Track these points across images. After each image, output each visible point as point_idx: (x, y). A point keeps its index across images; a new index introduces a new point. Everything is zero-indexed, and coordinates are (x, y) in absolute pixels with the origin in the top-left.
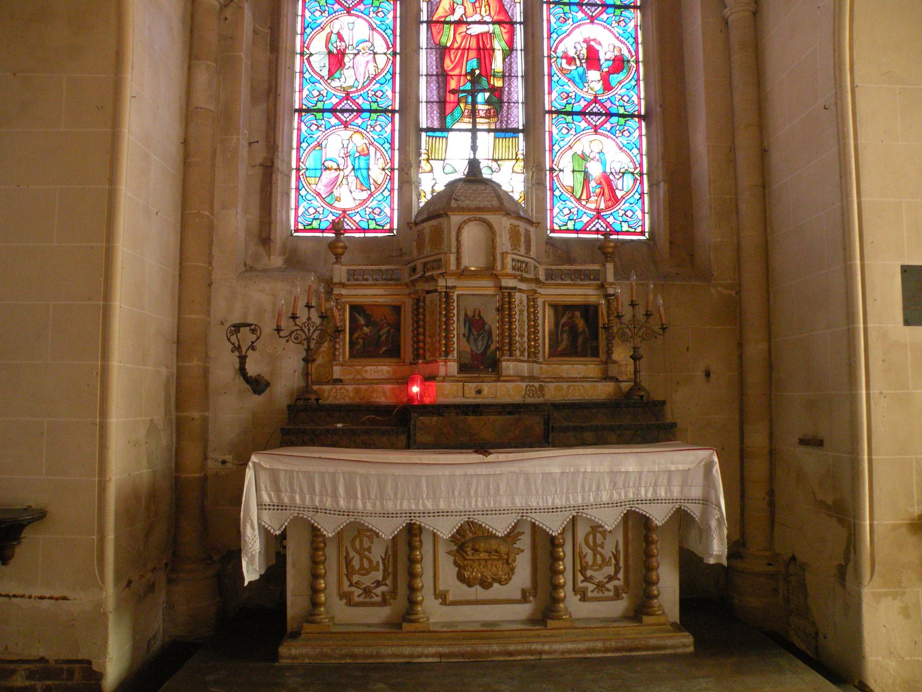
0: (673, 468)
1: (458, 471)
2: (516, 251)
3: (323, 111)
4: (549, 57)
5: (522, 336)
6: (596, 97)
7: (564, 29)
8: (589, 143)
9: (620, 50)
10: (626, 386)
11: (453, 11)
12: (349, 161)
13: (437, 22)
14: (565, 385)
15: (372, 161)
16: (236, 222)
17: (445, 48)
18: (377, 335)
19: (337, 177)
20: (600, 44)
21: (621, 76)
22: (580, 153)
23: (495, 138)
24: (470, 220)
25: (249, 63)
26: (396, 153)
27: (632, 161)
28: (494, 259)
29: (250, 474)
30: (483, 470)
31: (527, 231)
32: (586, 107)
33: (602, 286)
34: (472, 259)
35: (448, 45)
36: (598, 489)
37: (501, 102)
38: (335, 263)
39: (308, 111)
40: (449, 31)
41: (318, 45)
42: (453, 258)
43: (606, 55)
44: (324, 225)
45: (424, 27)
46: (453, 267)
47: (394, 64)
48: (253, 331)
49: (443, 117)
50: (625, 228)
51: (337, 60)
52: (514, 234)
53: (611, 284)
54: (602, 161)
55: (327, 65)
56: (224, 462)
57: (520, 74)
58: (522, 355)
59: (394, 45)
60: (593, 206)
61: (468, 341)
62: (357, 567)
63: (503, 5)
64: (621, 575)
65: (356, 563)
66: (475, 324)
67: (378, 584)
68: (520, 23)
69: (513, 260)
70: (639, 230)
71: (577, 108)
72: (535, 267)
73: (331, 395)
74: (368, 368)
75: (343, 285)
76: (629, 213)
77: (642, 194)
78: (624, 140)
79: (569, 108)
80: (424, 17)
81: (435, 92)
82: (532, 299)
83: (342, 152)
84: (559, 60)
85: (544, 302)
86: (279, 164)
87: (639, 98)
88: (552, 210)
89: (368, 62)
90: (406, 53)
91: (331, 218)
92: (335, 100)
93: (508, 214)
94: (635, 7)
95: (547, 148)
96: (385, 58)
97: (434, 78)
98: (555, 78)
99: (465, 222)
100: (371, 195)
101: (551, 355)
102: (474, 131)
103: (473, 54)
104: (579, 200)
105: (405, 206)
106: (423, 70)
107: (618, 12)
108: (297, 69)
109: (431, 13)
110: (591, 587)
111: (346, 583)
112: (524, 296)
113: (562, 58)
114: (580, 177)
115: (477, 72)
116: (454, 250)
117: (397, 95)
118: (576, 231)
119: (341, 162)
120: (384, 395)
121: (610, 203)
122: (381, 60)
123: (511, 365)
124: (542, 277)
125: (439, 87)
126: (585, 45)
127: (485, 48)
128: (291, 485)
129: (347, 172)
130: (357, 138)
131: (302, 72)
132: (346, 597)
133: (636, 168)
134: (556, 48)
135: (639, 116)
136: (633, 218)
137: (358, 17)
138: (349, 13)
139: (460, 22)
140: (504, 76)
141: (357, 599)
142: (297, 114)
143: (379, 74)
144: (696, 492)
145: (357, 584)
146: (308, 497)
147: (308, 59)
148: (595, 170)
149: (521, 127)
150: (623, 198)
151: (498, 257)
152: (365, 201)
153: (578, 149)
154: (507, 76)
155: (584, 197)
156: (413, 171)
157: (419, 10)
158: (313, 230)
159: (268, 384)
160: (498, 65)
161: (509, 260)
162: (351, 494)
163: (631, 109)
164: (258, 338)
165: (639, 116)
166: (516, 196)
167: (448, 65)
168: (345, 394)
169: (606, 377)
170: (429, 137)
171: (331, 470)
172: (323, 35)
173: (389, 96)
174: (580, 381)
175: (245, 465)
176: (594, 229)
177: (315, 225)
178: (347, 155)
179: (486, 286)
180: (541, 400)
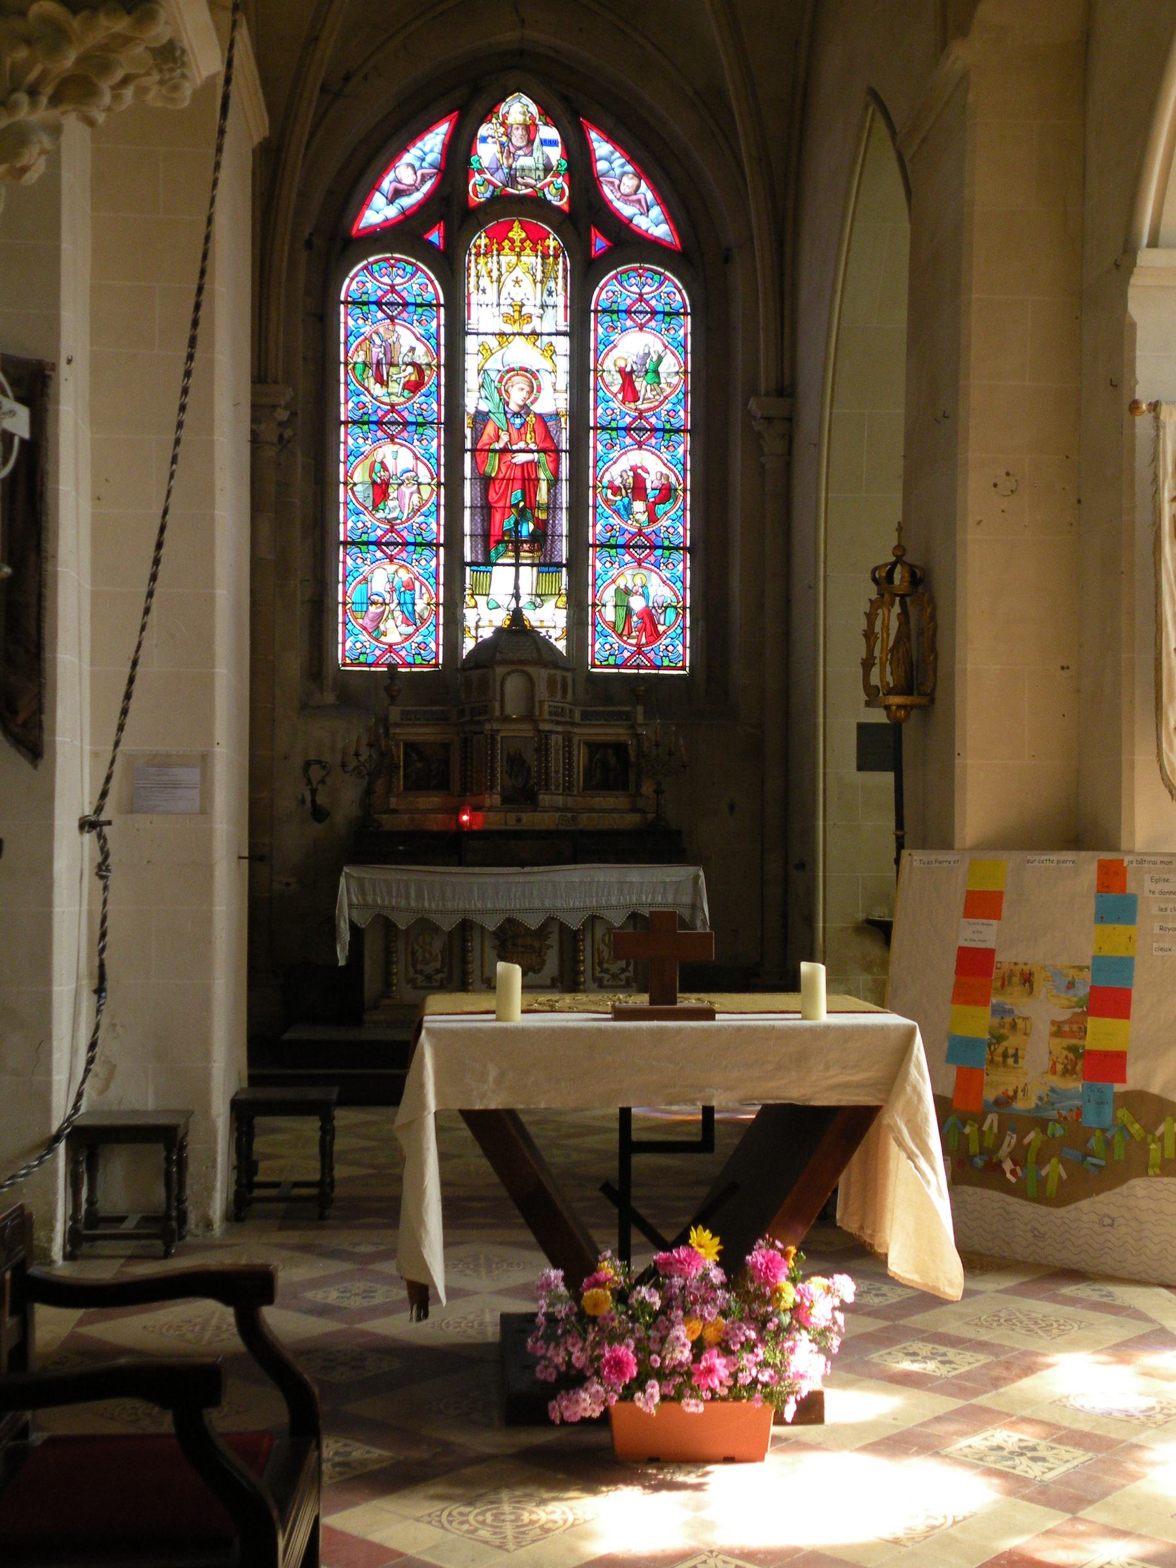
0: (668, 880)
1: (501, 880)
4: (595, 487)
5: (557, 772)
6: (640, 529)
7: (611, 456)
8: (629, 578)
9: (668, 478)
10: (650, 816)
11: (498, 438)
12: (395, 597)
13: (482, 450)
14: (595, 815)
15: (417, 595)
16: (293, 664)
17: (490, 478)
18: (431, 771)
19: (383, 612)
21: (667, 506)
22: (622, 587)
23: (539, 572)
26: (441, 588)
27: (677, 597)
28: (533, 707)
29: (342, 880)
30: (520, 879)
31: (564, 679)
32: (630, 540)
33: (632, 727)
34: (513, 707)
36: (609, 895)
37: (545, 535)
39: (353, 543)
40: (494, 460)
41: (360, 475)
42: (497, 705)
43: (652, 481)
45: (468, 457)
46: (497, 713)
47: (438, 495)
48: (324, 767)
49: (487, 553)
51: (381, 490)
52: (552, 682)
53: (641, 725)
56: (288, 884)
57: (564, 506)
58: (557, 788)
59: (438, 475)
60: (634, 641)
61: (510, 776)
62: (420, 958)
64: (631, 968)
65: (419, 956)
66: (516, 762)
67: (437, 971)
68: (566, 451)
70: (680, 664)
72: (571, 710)
73: (389, 823)
74: (420, 800)
75: (398, 725)
76: (670, 648)
77: (684, 628)
78: (666, 573)
79: (613, 541)
80: (468, 445)
82: (568, 739)
85: (579, 741)
87: (685, 529)
88: (593, 646)
89: (412, 494)
90: (452, 483)
92: (379, 533)
93: (545, 666)
94: (686, 431)
95: (590, 582)
96: (428, 489)
98: (600, 510)
99: (509, 673)
101: (585, 789)
103: (518, 484)
104: (620, 636)
106: (467, 502)
108: (342, 499)
109: (475, 441)
110: (607, 977)
111: (411, 970)
112: (560, 737)
114: (622, 612)
115: (522, 504)
116: (498, 698)
117: (442, 528)
118: (616, 666)
119: (387, 597)
120: (436, 822)
121: (651, 639)
122: (426, 491)
123: (547, 797)
124: (577, 717)
125: (483, 520)
126: (631, 474)
127: (530, 479)
128: (374, 891)
129: (393, 606)
130: (402, 572)
131: (346, 503)
132: (411, 981)
133: (678, 602)
134: (602, 477)
135: (684, 549)
136: (674, 651)
137: (402, 445)
138: (393, 441)
139: (505, 451)
140: (548, 508)
141: (420, 984)
142: (341, 548)
143: (424, 505)
144: (686, 899)
145: (421, 972)
146: (387, 899)
147: (352, 489)
148: (637, 604)
149: (564, 562)
150: (664, 632)
151: (537, 705)
152: (410, 636)
153: (621, 583)
154: (552, 507)
155: (626, 632)
157: (464, 437)
158: (360, 664)
159: (328, 814)
160: (542, 496)
161: (546, 707)
162: (420, 897)
163: (677, 541)
164: (328, 774)
165: (684, 549)
166: (669, 239)
167: (493, 496)
168: (402, 822)
169: (634, 810)
171: (405, 878)
172: (368, 462)
173: (435, 528)
174: (610, 811)
175: (339, 874)
177: (362, 659)
178: (393, 589)
179: (526, 730)
180: (573, 828)
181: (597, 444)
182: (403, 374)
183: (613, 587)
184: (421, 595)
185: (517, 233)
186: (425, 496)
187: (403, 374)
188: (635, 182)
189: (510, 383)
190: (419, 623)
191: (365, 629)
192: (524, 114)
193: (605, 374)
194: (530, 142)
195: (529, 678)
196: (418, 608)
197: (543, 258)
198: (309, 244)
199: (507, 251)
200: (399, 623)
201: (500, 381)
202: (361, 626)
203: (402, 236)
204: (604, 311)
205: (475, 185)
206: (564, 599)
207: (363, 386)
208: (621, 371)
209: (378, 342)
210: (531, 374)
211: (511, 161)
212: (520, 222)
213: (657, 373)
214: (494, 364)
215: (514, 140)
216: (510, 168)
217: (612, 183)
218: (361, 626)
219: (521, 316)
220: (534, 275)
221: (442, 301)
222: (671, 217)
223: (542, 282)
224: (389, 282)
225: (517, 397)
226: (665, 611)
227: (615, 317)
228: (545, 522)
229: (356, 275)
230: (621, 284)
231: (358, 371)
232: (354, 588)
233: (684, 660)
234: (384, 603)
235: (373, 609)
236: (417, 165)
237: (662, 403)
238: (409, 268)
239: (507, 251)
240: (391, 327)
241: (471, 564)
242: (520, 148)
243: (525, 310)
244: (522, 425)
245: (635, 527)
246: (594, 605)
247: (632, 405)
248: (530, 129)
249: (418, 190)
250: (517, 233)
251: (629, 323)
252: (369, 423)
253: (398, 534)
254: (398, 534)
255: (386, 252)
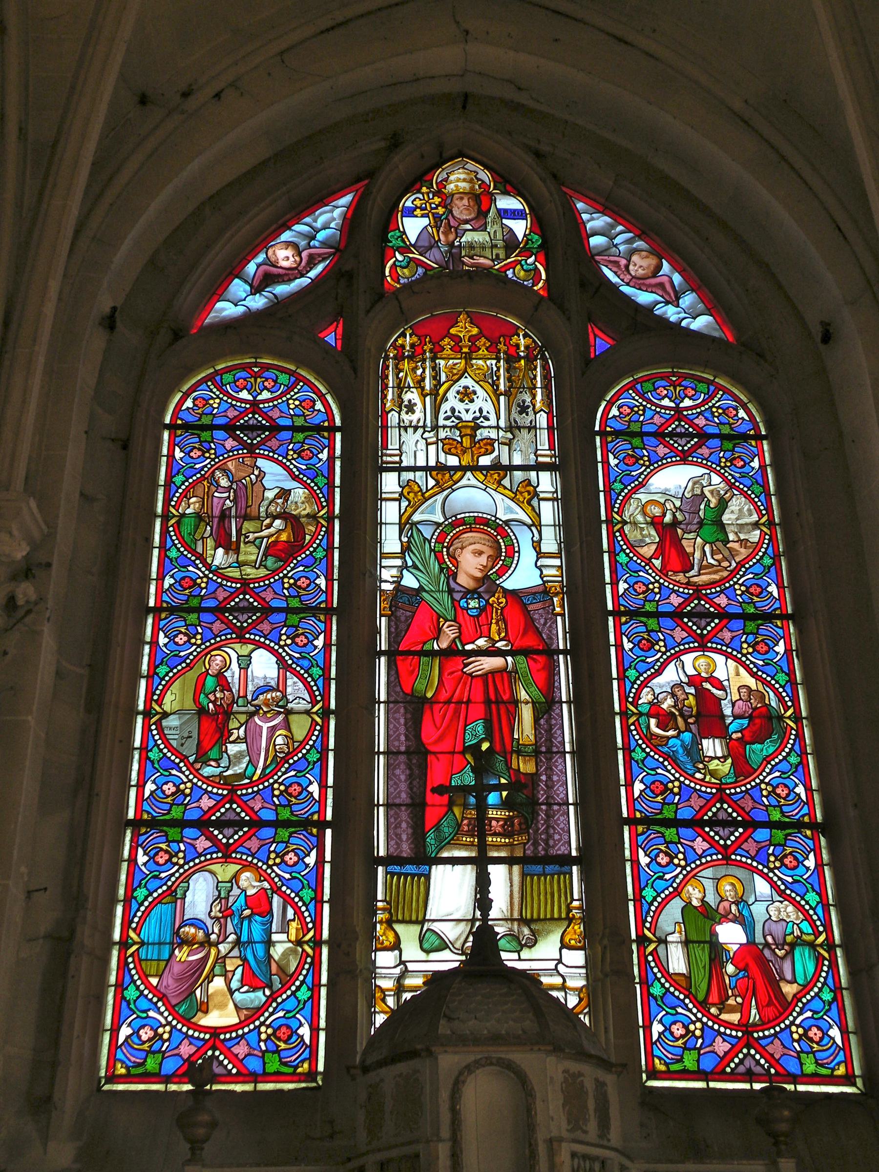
2: (579, 1135)
3: (182, 824)
6: (721, 789)
11: (438, 634)
13: (408, 653)
20: (722, 688)
21: (768, 748)
23: (523, 875)
24: (478, 1064)
25: (43, 735)
27: (808, 918)
28: (533, 1155)
31: (600, 1085)
35: (429, 695)
37: (534, 803)
38: (189, 1162)
44: (170, 1066)
47: (324, 732)
50: (810, 1067)
51: (215, 722)
54: (745, 922)
55: (195, 735)
63: (533, 620)
68: (565, 652)
69: (574, 1155)
70: (841, 1071)
71: (685, 813)
79: (668, 813)
81: (403, 786)
83: (216, 909)
84: (642, 720)
86: (86, 936)
91: (186, 1050)
94: (784, 617)
96: (306, 721)
97: (402, 758)
99: (469, 1069)
100: (271, 998)
102: (481, 863)
103: (478, 709)
104: (703, 1005)
105: (342, 1026)
107: (751, 626)
113: (649, 715)
114: (703, 955)
115: (485, 746)
116: (445, 1133)
121: (770, 1012)
122: (300, 727)
125: (410, 777)
129: (223, 948)
130: (247, 879)
134: (637, 696)
140: (537, 753)
147: (158, 724)
150: (797, 997)
151: (542, 1149)
152: (259, 1011)
153: (694, 894)
154: (545, 749)
155: (714, 998)
156: (359, 947)
158: (147, 1077)
160: (526, 726)
167: (429, 734)
170: (393, 874)
172: (192, 676)
173: (318, 791)
176: (741, 1069)
177: (151, 1064)
178: (227, 913)
181: (620, 641)
182: (265, 533)
183: (676, 905)
184: (284, 930)
185: (464, 329)
186: (299, 733)
187: (265, 533)
188: (652, 261)
189: (457, 544)
190: (277, 985)
191: (163, 997)
192: (471, 181)
193: (627, 528)
194: (482, 214)
195: (521, 1079)
196: (277, 952)
197: (507, 361)
198: (110, 322)
199: (448, 352)
200: (235, 984)
201: (440, 540)
202: (153, 989)
203: (274, 331)
204: (617, 433)
205: (394, 266)
206: (579, 928)
207: (194, 552)
208: (656, 522)
209: (224, 482)
210: (496, 532)
211: (451, 237)
212: (467, 313)
213: (722, 527)
214: (431, 514)
215: (456, 212)
216: (451, 245)
217: (616, 263)
218: (153, 989)
219: (474, 442)
220: (495, 385)
221: (338, 422)
222: (712, 304)
223: (507, 394)
224: (250, 398)
225: (471, 563)
226: (790, 953)
227: (637, 442)
228: (534, 778)
229: (193, 389)
230: (642, 396)
231: (186, 529)
232: (149, 910)
233: (848, 1062)
234: (206, 943)
235: (181, 954)
236: (303, 243)
237: (734, 573)
238: (283, 378)
239: (448, 352)
240: (248, 461)
241: (386, 861)
242: (466, 222)
243: (481, 434)
244: (482, 610)
245: (710, 785)
246: (642, 940)
247: (680, 577)
248: (481, 201)
249: (302, 276)
250: (464, 329)
251: (662, 450)
252: (199, 610)
253: (245, 806)
254: (245, 806)
255: (243, 353)
